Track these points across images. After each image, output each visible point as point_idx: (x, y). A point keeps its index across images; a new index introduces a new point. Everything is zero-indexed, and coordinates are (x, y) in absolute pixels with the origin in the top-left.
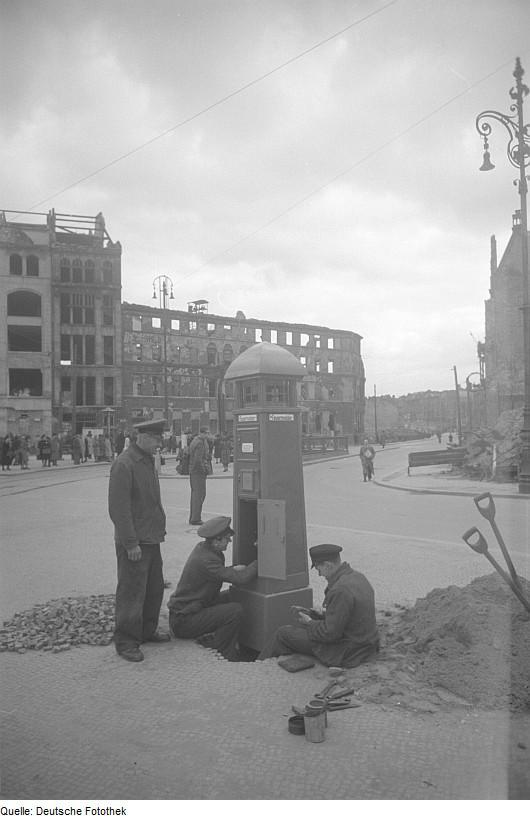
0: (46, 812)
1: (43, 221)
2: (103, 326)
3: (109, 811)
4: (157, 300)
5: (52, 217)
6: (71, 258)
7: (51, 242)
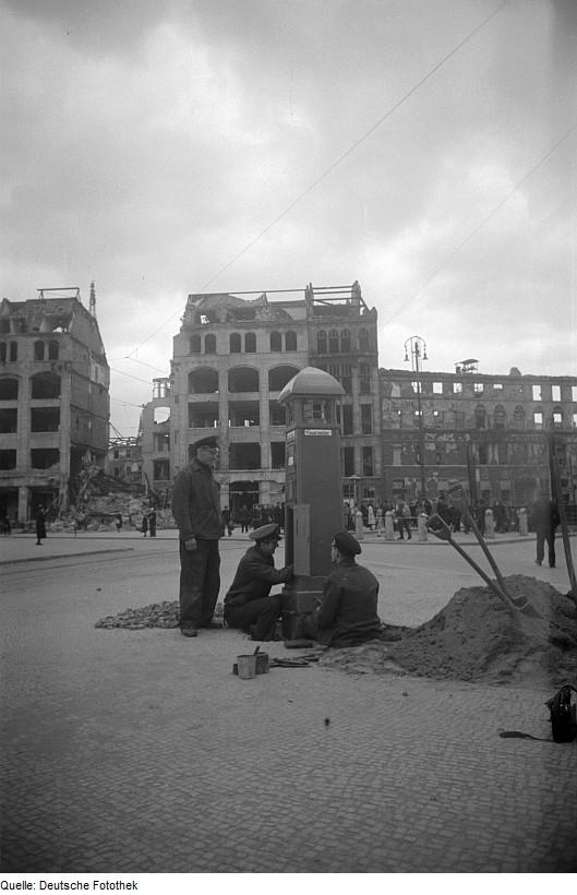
0: (50, 886)
1: (301, 296)
2: (360, 395)
3: (119, 885)
4: (410, 363)
5: (309, 292)
6: (328, 330)
7: (308, 315)
